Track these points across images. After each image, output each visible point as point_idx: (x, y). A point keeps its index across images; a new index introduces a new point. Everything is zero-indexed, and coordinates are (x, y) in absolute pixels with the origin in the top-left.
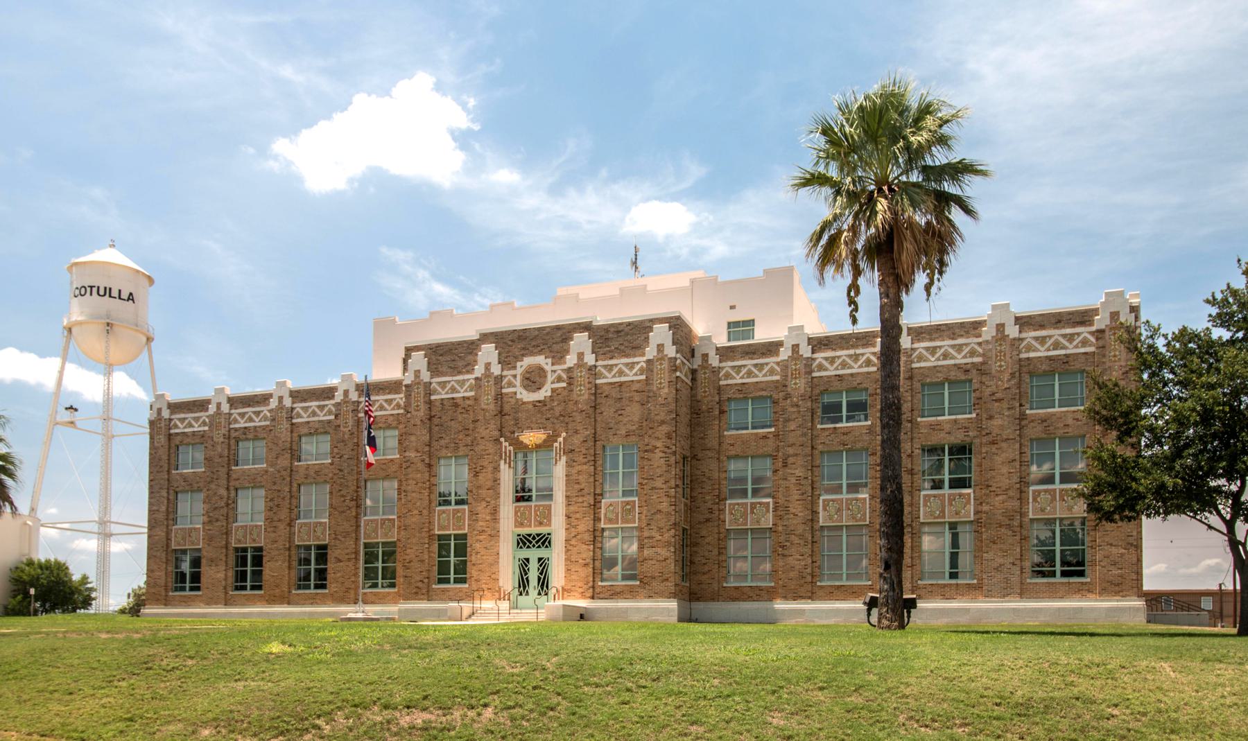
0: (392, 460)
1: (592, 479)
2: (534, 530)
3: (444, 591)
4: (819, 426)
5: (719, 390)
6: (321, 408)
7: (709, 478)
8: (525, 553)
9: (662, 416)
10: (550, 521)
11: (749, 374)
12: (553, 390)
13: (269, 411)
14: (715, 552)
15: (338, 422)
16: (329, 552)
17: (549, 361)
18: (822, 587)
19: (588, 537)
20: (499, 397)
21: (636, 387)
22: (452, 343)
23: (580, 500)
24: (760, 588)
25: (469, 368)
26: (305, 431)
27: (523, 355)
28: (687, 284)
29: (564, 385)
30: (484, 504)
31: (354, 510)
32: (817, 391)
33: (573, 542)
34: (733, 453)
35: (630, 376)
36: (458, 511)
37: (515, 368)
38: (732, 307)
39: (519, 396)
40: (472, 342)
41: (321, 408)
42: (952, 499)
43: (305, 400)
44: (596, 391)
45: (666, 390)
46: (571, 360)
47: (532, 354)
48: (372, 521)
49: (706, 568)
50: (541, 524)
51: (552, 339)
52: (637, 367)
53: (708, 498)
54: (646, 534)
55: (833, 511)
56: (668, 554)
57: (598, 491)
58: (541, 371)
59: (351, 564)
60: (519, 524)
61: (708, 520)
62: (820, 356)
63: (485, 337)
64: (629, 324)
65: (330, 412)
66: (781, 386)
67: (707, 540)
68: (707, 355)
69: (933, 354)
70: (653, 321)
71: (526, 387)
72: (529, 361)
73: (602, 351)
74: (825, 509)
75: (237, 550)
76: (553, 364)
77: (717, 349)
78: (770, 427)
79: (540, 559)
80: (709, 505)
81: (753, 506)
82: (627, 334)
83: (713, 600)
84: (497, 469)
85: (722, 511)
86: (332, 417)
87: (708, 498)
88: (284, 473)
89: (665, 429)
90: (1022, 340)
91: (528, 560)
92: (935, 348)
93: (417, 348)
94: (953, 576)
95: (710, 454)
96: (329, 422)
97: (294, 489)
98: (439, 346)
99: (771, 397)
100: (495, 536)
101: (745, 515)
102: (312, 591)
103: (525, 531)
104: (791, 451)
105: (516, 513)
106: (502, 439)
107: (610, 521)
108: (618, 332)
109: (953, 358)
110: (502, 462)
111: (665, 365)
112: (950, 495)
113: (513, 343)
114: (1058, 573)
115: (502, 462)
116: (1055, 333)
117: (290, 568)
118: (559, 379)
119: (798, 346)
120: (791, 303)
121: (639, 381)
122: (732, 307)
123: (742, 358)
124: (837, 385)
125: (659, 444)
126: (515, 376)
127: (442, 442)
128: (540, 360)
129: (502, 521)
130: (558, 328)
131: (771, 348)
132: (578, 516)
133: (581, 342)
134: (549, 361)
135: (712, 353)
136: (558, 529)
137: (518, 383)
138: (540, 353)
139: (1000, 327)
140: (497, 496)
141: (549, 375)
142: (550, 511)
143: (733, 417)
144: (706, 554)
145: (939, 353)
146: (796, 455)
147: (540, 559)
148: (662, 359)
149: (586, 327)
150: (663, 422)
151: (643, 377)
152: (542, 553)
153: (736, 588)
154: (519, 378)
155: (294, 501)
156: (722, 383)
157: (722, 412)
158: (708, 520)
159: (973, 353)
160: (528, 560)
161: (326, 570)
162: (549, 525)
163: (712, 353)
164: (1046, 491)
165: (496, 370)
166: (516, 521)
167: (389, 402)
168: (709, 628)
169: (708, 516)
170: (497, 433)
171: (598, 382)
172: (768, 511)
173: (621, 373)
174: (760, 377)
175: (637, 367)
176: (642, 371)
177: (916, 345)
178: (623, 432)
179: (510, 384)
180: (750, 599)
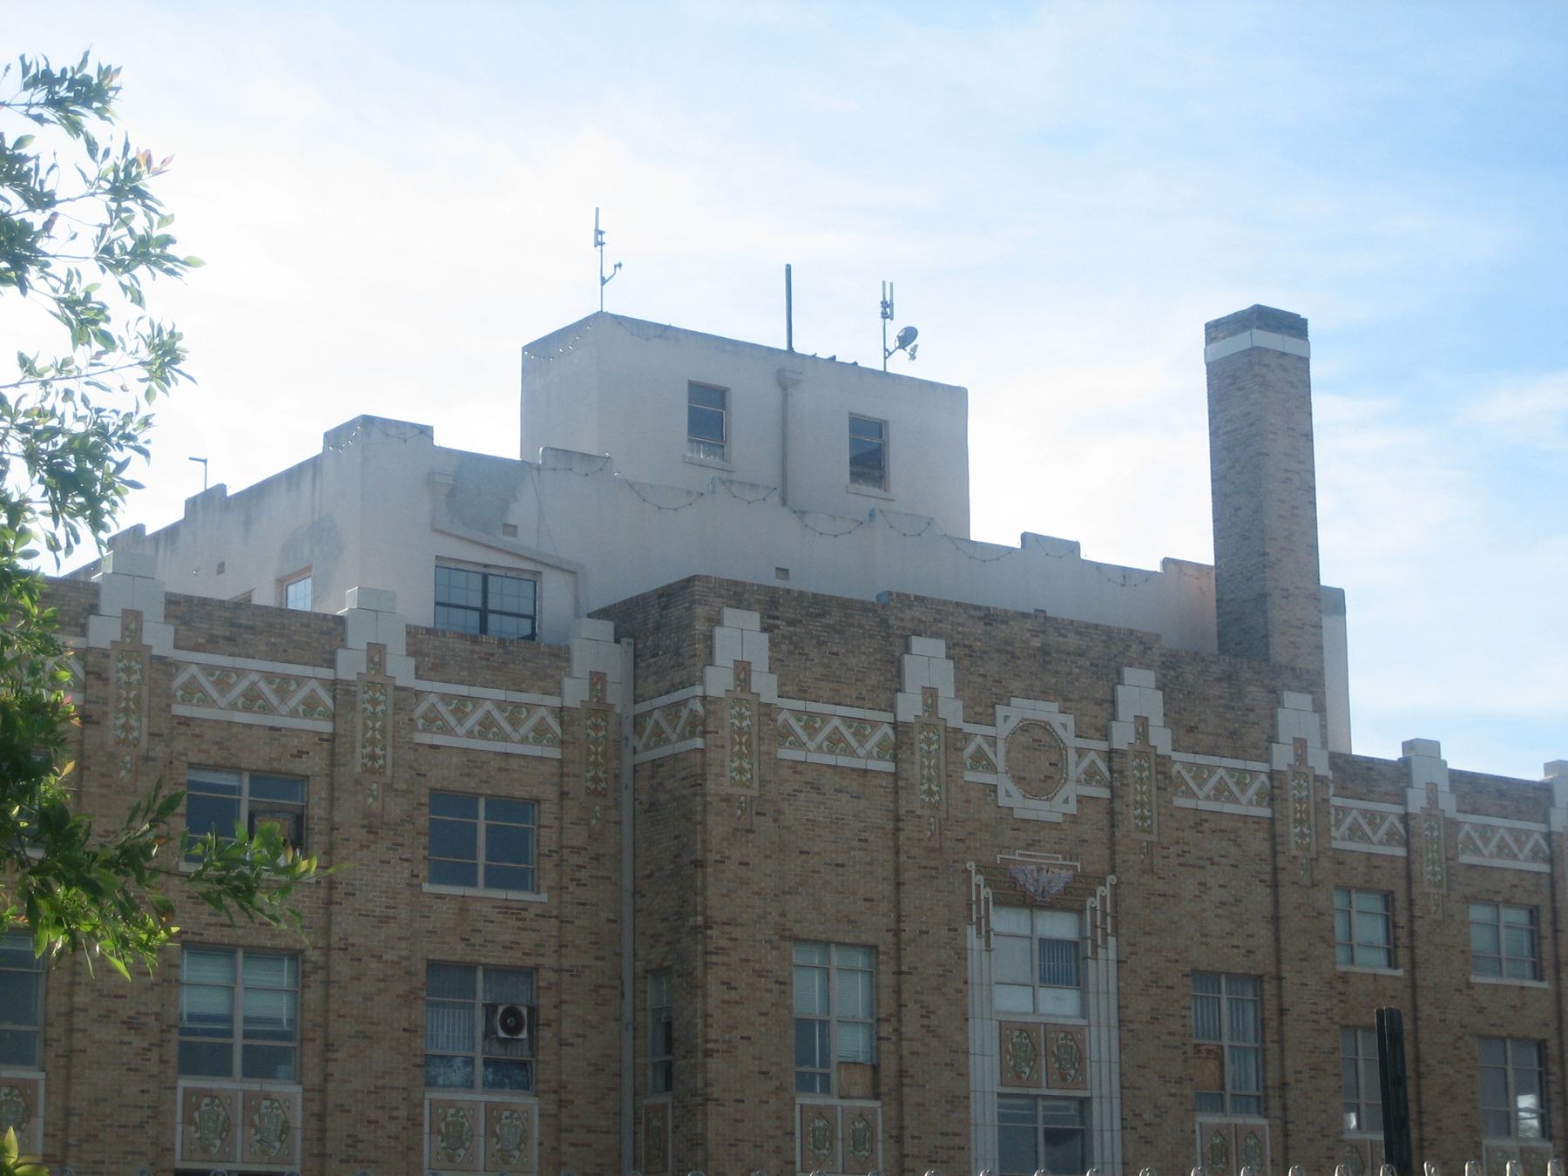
126: (993, 741)
141: (1072, 756)
154: (1001, 744)
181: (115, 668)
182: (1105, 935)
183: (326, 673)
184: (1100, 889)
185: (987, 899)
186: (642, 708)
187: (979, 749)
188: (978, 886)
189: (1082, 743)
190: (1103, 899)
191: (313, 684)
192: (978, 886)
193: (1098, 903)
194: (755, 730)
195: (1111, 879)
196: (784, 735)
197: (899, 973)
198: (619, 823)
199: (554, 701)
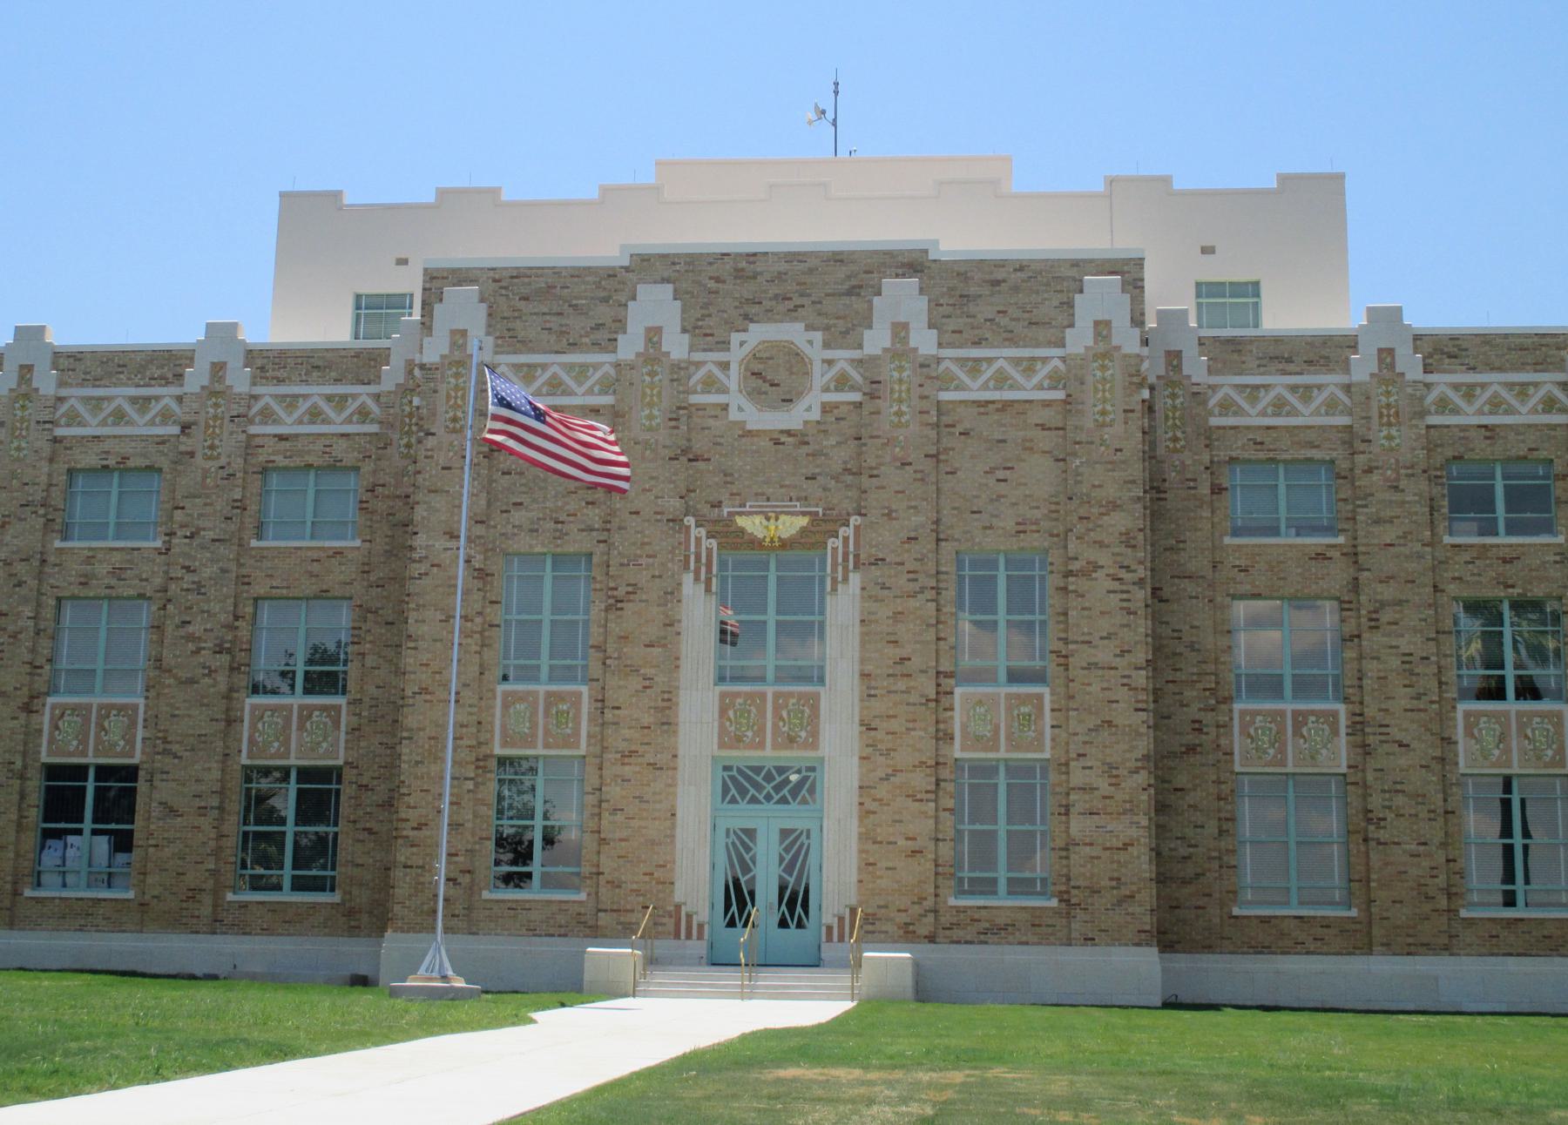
0: (338, 553)
1: (930, 635)
2: (769, 755)
3: (513, 907)
4: (1447, 539)
5: (1210, 437)
6: (143, 403)
7: (1192, 647)
8: (743, 815)
9: (1111, 491)
10: (815, 734)
11: (1279, 406)
12: (827, 408)
13: (377, 397)
14: (1212, 828)
15: (186, 444)
16: (142, 786)
17: (818, 336)
18: (1470, 922)
19: (921, 781)
20: (681, 413)
21: (1045, 416)
22: (556, 272)
23: (901, 685)
24: (1326, 923)
25: (602, 335)
26: (90, 459)
27: (748, 318)
28: (1100, 187)
29: (856, 397)
30: (635, 683)
31: (222, 678)
32: (1438, 460)
33: (882, 791)
34: (1247, 588)
35: (1028, 390)
36: (560, 697)
37: (724, 345)
38: (1207, 250)
39: (734, 415)
40: (611, 274)
41: (143, 403)
42: (306, 713)
43: (96, 381)
44: (942, 420)
45: (1119, 428)
46: (876, 340)
47: (769, 316)
48: (75, 708)
49: (1190, 870)
50: (791, 740)
51: (833, 285)
52: (1043, 372)
53: (1189, 694)
54: (1078, 777)
55: (1490, 740)
56: (1134, 832)
57: (945, 666)
58: (795, 360)
59: (205, 823)
60: (730, 739)
61: (1191, 749)
62: (1442, 381)
63: (647, 266)
64: (1021, 267)
65: (166, 417)
66: (1351, 439)
67: (1191, 798)
68: (1178, 354)
69: (1253, 400)
70: (1081, 266)
71: (755, 395)
72: (760, 333)
73: (952, 325)
74: (1469, 733)
75: (53, 771)
76: (827, 345)
77: (1417, 338)
78: (1330, 530)
79: (785, 833)
80: (1193, 711)
81: (1300, 719)
82: (1016, 289)
83: (1208, 948)
84: (672, 594)
85: (1225, 726)
86: (176, 430)
87: (1189, 694)
88: (20, 568)
89: (1120, 522)
90: (255, 398)
91: (750, 833)
92: (148, 399)
93: (460, 276)
94: (1510, 900)
95: (1190, 587)
96: (162, 441)
97: (48, 613)
98: (519, 275)
99: (1339, 466)
100: (665, 767)
101: (1278, 740)
102: (287, 896)
103: (743, 756)
104: (1388, 592)
105: (723, 712)
106: (690, 521)
107: (978, 741)
108: (996, 283)
109: (1239, 412)
110: (688, 578)
111: (1115, 371)
112: (302, 708)
113: (725, 286)
114: (1002, 886)
115: (688, 578)
116: (317, 391)
117: (20, 827)
118: (842, 383)
119: (30, 368)
120: (1344, 249)
121: (1047, 404)
122: (1207, 250)
123: (1262, 368)
124: (1481, 448)
125: (1103, 558)
126: (725, 366)
127: (518, 516)
128: (792, 332)
129: (682, 730)
130: (838, 258)
131: (1326, 351)
132: (894, 725)
133: (902, 300)
134: (818, 336)
135: (235, 363)
136: (839, 753)
137: (733, 379)
138: (793, 313)
139: (1386, 356)
140: (674, 663)
141: (817, 368)
142: (815, 709)
143: (1238, 505)
144: (1189, 832)
145: (1266, 399)
146: (1400, 603)
147: (785, 833)
148: (1105, 355)
149: (913, 264)
150: (1114, 506)
151: (1059, 395)
152: (794, 816)
153: (1265, 920)
154: (734, 367)
155: (45, 646)
156: (1214, 421)
157: (1217, 490)
158: (1191, 749)
159: (363, 414)
160: (750, 833)
161: (132, 831)
162: (814, 745)
163: (235, 363)
164: (324, 708)
165: (676, 346)
166: (722, 731)
167: (340, 401)
168: (946, 1009)
169: (1191, 738)
170: (674, 504)
171: (945, 396)
172: (1335, 732)
173: (1001, 380)
174: (1307, 416)
175: (1043, 372)
176: (1056, 380)
177: (258, 390)
178: (1010, 525)
179: (710, 384)
180: (1296, 947)
181: (889, 373)
182: (846, 570)
183: (1342, 379)
184: (842, 531)
185: (709, 551)
186: (64, 392)
187: (710, 375)
188: (698, 540)
189: (829, 354)
190: (846, 539)
191: (1001, 363)
192: (698, 540)
193: (839, 543)
194: (1375, 427)
195: (855, 520)
196: (947, 381)
197: (936, 911)
198: (64, 885)
199: (1342, 379)
